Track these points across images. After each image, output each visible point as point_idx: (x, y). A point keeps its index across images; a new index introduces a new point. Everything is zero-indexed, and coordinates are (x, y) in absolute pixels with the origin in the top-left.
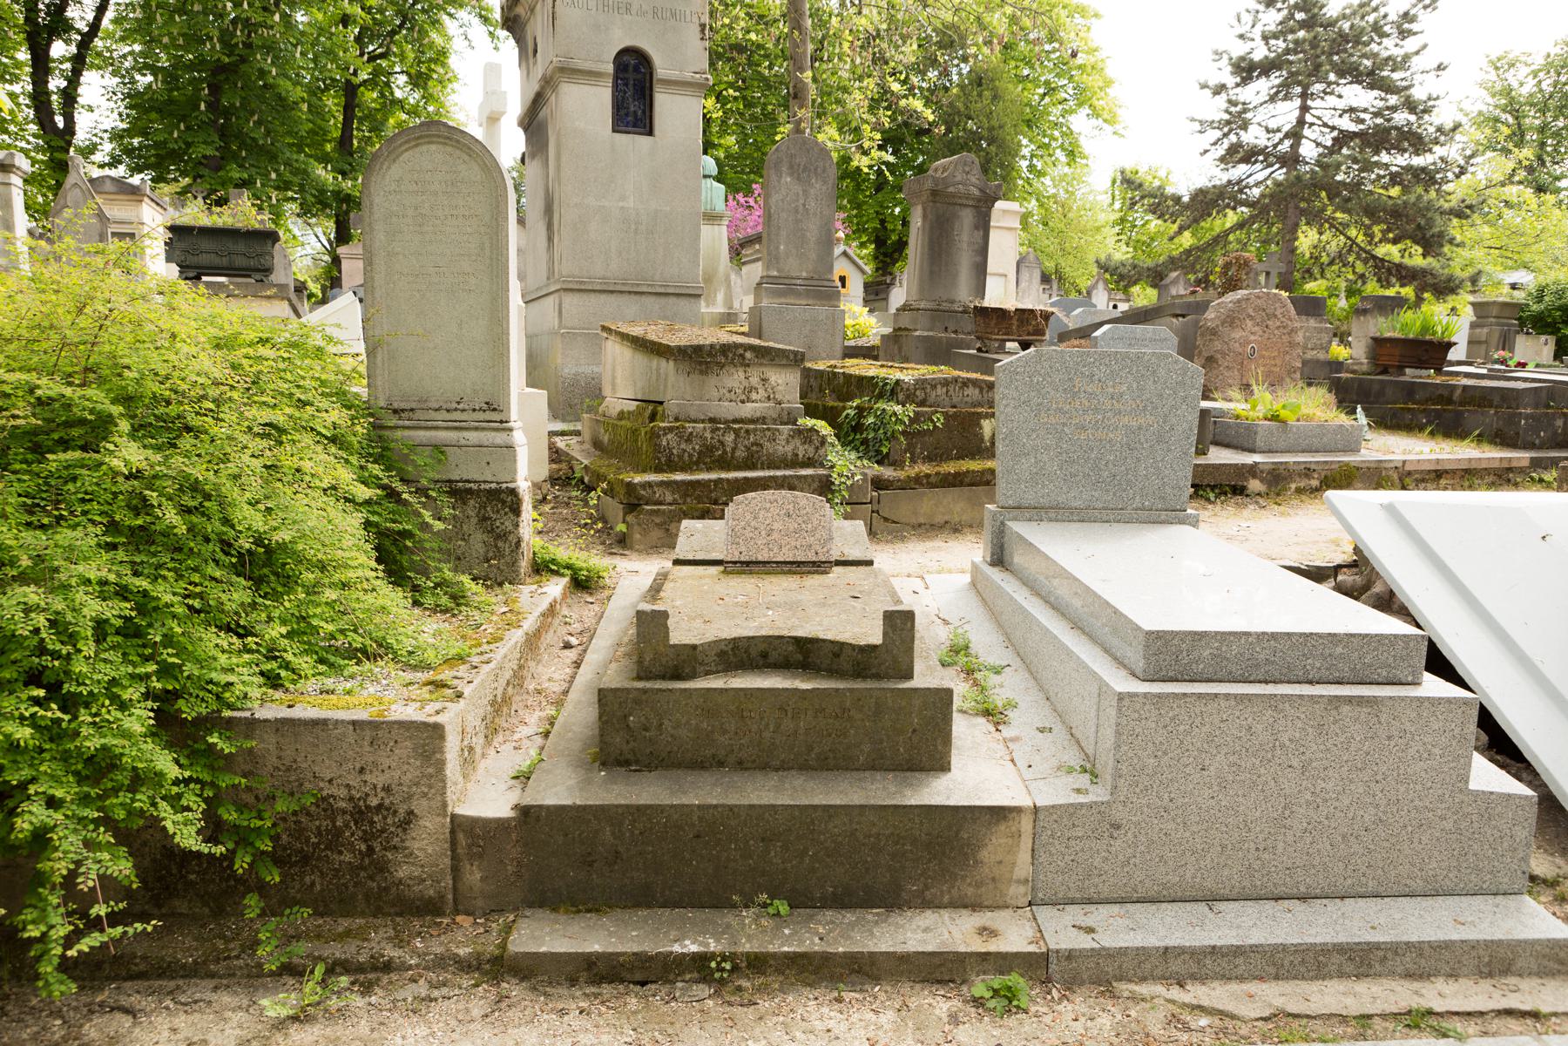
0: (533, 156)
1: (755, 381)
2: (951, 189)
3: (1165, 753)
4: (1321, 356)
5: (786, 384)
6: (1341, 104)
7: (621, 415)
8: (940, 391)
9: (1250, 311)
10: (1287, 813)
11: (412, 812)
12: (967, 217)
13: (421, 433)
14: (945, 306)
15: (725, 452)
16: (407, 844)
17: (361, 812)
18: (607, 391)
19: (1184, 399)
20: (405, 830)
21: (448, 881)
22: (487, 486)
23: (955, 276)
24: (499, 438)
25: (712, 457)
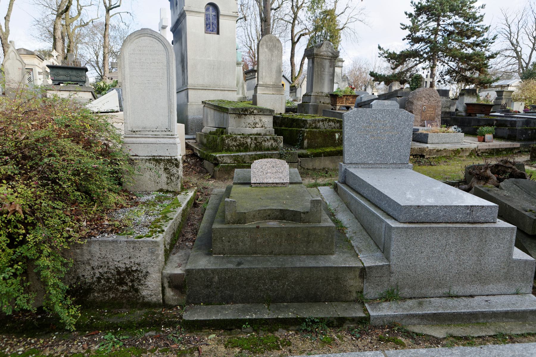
0: (176, 42)
1: (257, 120)
2: (322, 53)
3: (409, 248)
4: (448, 110)
5: (268, 121)
7: (211, 133)
8: (321, 123)
9: (424, 95)
10: (450, 267)
11: (147, 272)
12: (327, 63)
13: (143, 139)
14: (320, 94)
15: (248, 145)
16: (146, 283)
17: (130, 272)
18: (205, 124)
19: (408, 125)
20: (145, 278)
21: (161, 295)
22: (167, 158)
24: (171, 141)
25: (245, 147)
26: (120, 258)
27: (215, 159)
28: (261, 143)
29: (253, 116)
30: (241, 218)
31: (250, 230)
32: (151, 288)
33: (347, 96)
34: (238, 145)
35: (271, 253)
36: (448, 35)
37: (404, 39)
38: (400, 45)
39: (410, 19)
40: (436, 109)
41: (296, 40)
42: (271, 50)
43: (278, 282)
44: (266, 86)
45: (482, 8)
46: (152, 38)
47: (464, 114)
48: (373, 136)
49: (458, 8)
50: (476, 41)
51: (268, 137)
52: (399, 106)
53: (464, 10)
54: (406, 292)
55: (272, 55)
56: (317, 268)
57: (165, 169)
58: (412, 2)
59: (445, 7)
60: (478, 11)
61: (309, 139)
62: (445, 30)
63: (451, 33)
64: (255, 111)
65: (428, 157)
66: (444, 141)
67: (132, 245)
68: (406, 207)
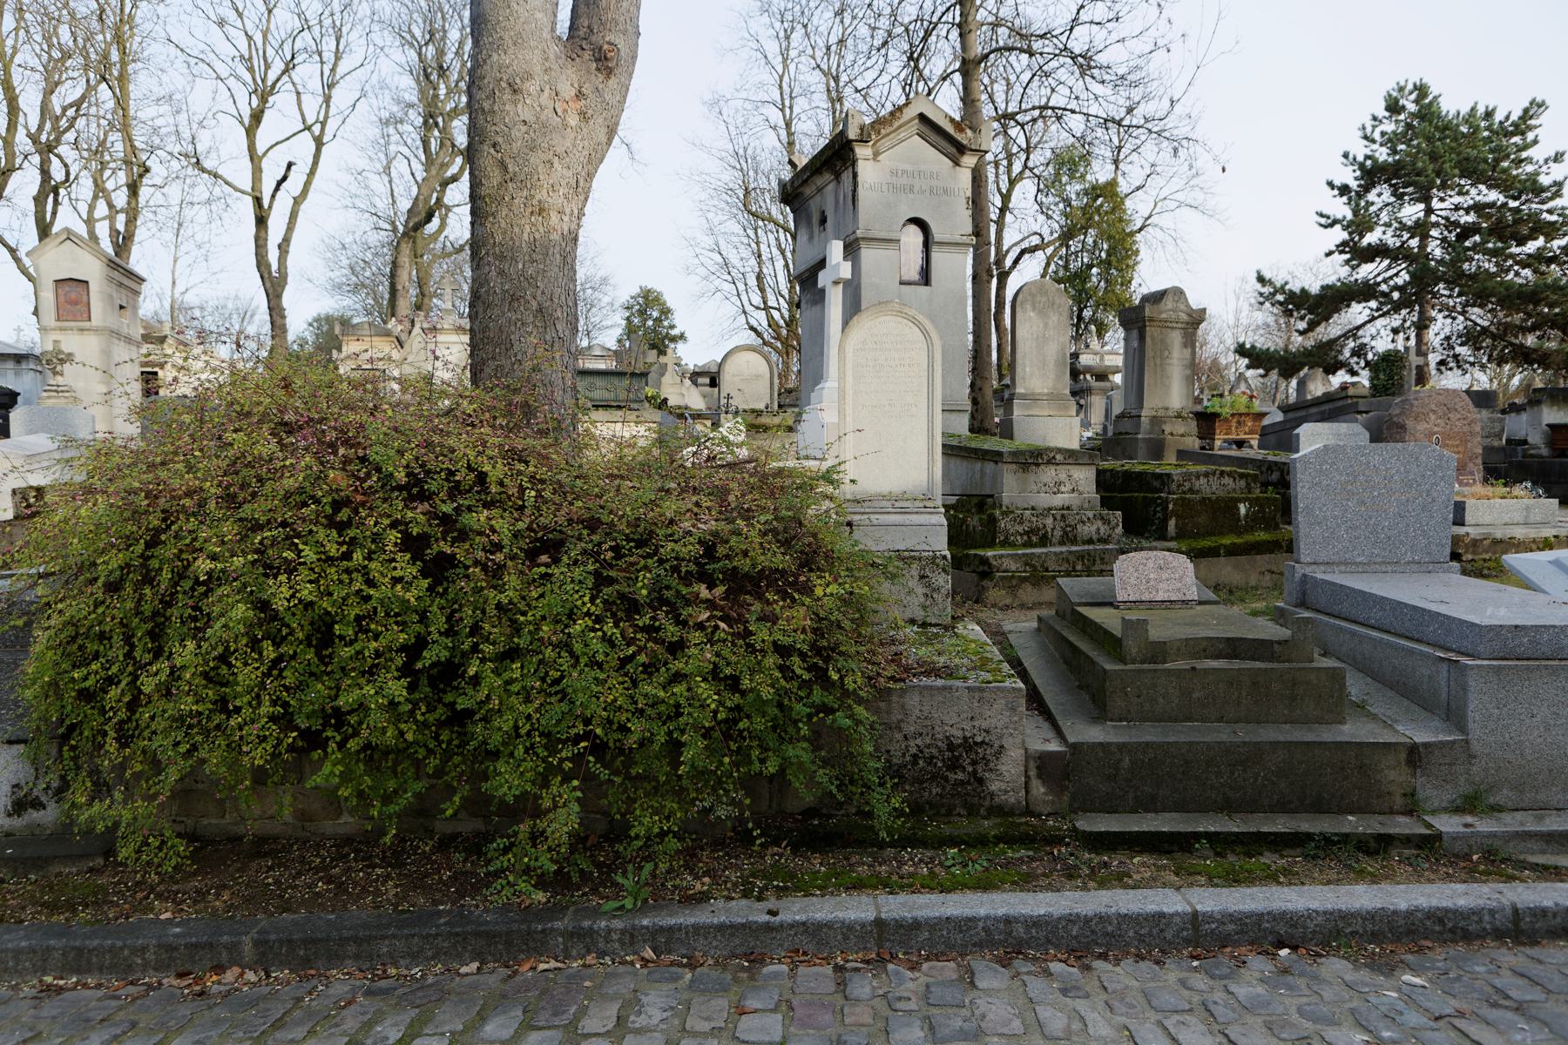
1: (1063, 476)
6: (1467, 201)
8: (1203, 480)
12: (1176, 338)
19: (1442, 478)
23: (1168, 387)
26: (955, 719)
27: (984, 561)
28: (1074, 527)
29: (1053, 468)
30: (1158, 652)
31: (1178, 673)
32: (1008, 777)
33: (1241, 415)
34: (1027, 533)
35: (1220, 720)
36: (1458, 236)
37: (1329, 254)
38: (1314, 263)
39: (1345, 199)
40: (1467, 441)
41: (1008, 262)
43: (1244, 771)
45: (1556, 160)
47: (1545, 451)
48: (1363, 503)
49: (1482, 166)
50: (1544, 248)
51: (1090, 514)
52: (1367, 435)
53: (1505, 171)
54: (1503, 796)
56: (1320, 743)
57: (922, 577)
58: (1346, 156)
59: (1447, 165)
60: (1544, 169)
61: (1178, 517)
62: (1450, 224)
63: (1467, 231)
64: (1058, 457)
65: (1470, 557)
66: (1506, 519)
67: (977, 695)
68: (1491, 628)
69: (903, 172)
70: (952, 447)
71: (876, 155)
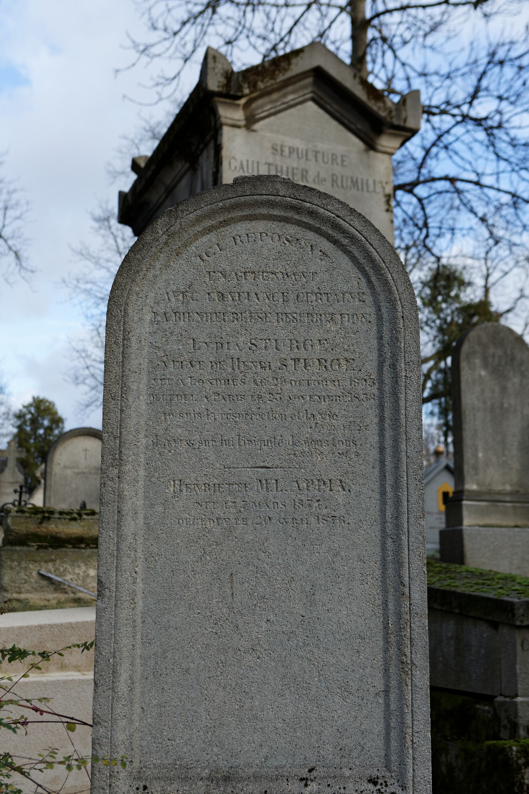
42: (498, 372)
44: (491, 498)
46: (291, 230)
55: (504, 389)
69: (292, 150)
70: (437, 591)
71: (250, 122)
